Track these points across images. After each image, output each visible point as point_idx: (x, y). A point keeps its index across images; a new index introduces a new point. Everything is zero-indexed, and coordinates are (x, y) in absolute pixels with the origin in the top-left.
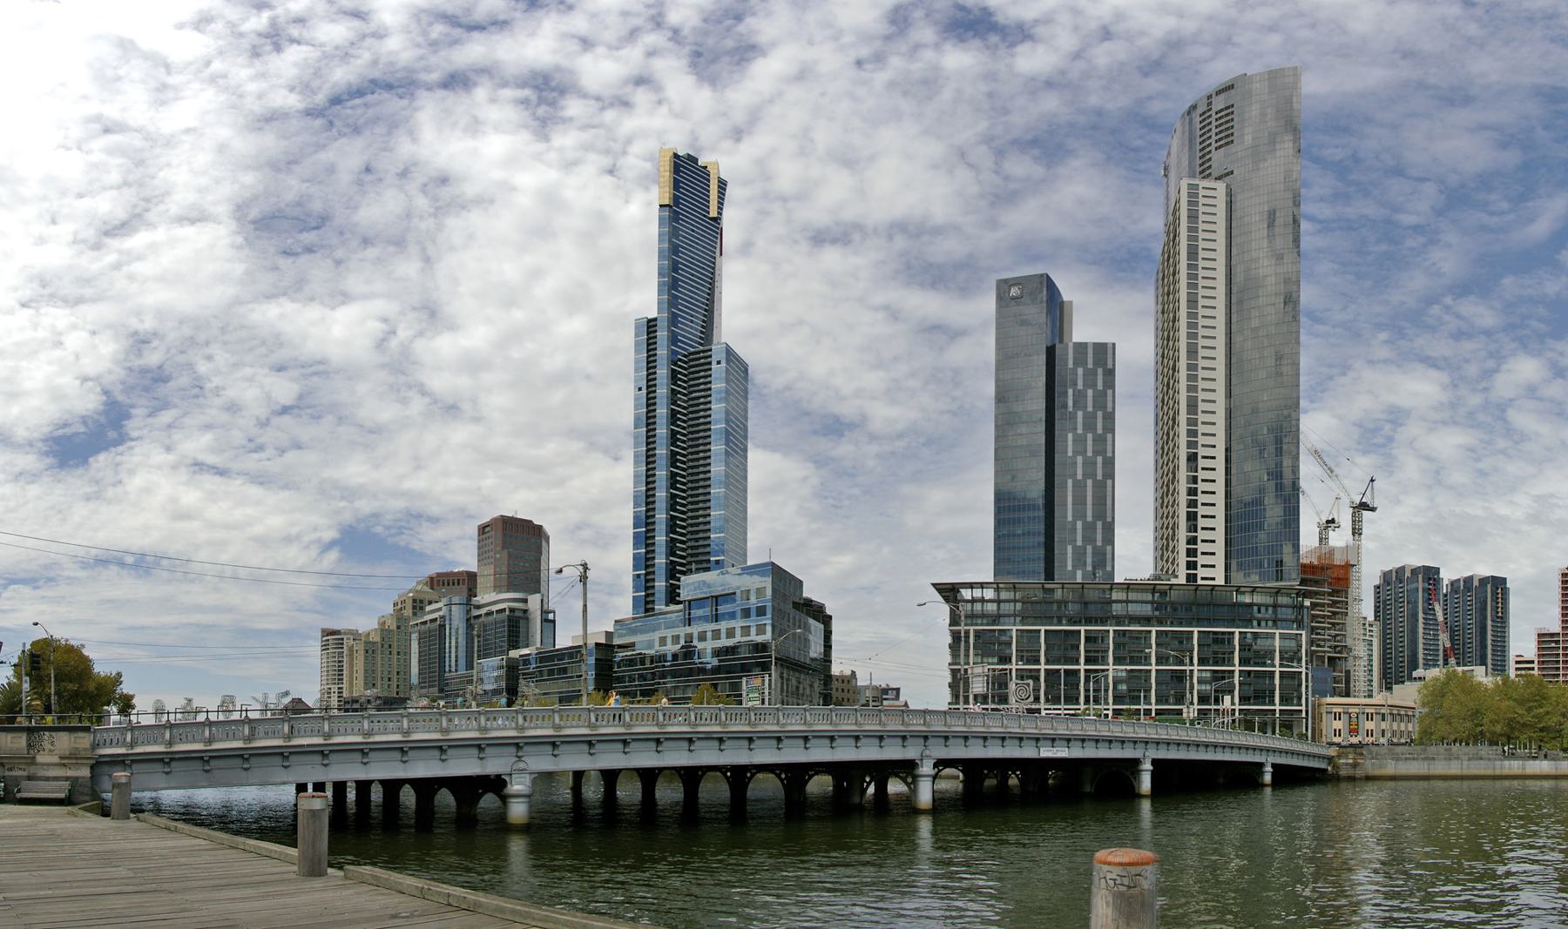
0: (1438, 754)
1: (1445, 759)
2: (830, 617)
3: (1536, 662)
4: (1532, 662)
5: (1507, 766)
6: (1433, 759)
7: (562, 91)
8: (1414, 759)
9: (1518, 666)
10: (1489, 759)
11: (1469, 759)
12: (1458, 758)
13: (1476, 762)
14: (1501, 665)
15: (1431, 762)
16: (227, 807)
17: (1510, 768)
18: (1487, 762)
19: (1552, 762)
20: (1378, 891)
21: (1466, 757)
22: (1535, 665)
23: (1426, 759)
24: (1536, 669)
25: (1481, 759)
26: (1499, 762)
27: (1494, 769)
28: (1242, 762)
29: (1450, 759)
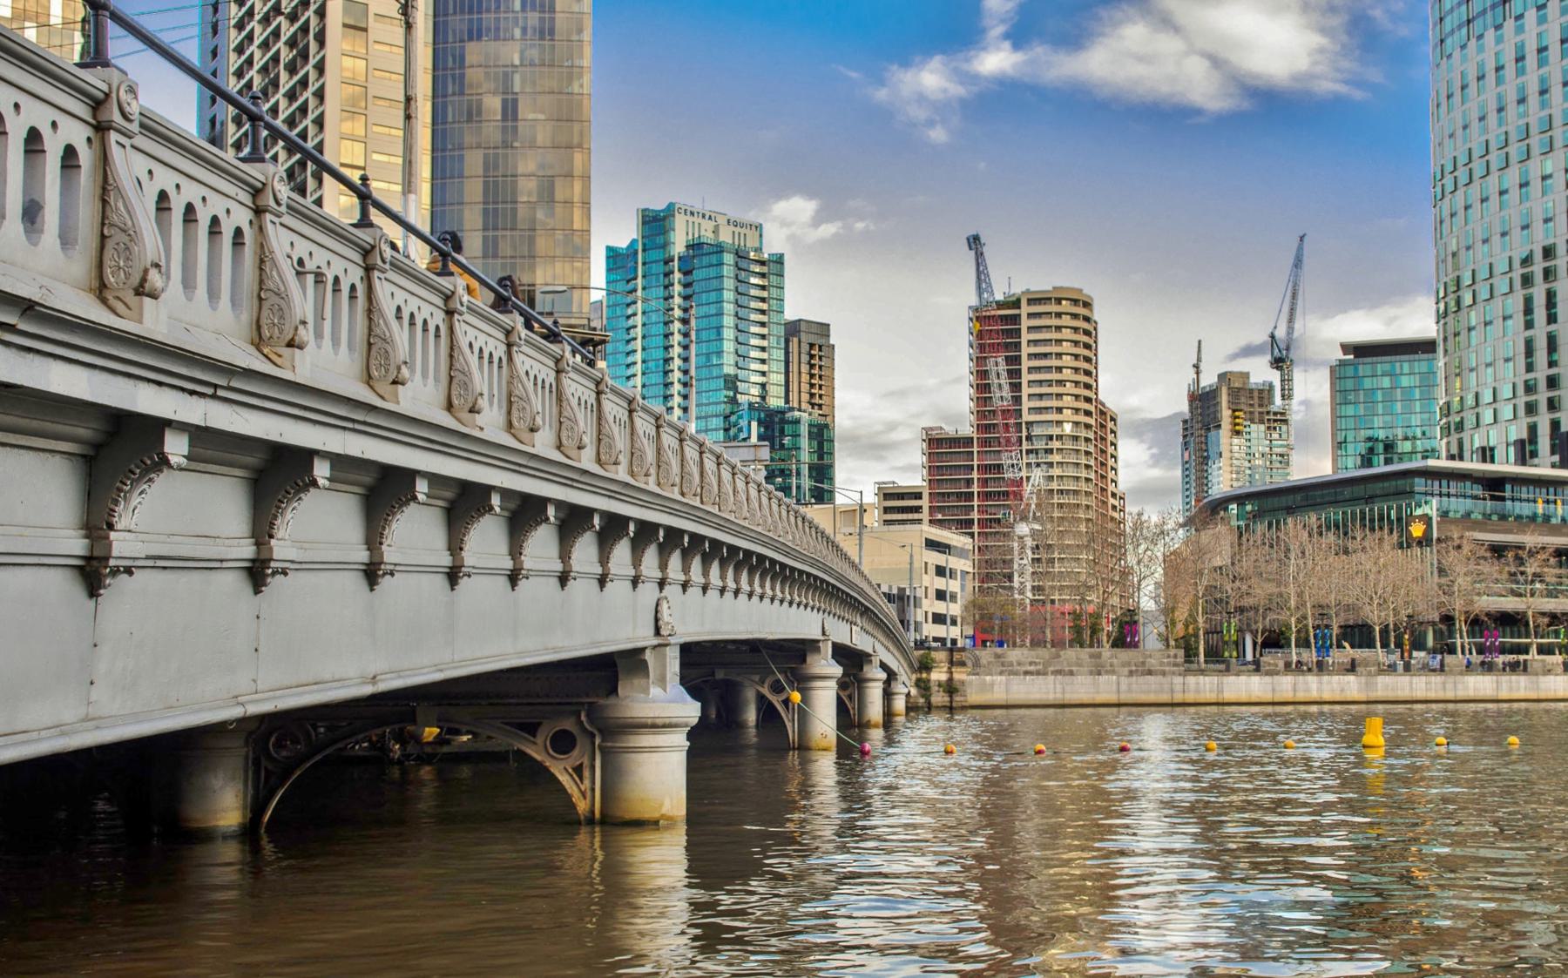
0: (1079, 665)
1: (1091, 673)
2: (1219, 376)
3: (926, 496)
4: (918, 496)
5: (1192, 687)
6: (1071, 673)
7: (373, 269)
8: (1038, 673)
9: (889, 517)
10: (1164, 674)
11: (1131, 673)
12: (1113, 672)
13: (1141, 679)
14: (959, 496)
15: (1068, 678)
16: (804, 748)
17: (1197, 691)
18: (1160, 678)
19: (1267, 679)
20: (729, 824)
21: (1126, 670)
22: (925, 503)
23: (1057, 672)
24: (926, 510)
25: (1150, 673)
26: (1178, 680)
27: (1172, 691)
28: (501, 671)
29: (1099, 674)
